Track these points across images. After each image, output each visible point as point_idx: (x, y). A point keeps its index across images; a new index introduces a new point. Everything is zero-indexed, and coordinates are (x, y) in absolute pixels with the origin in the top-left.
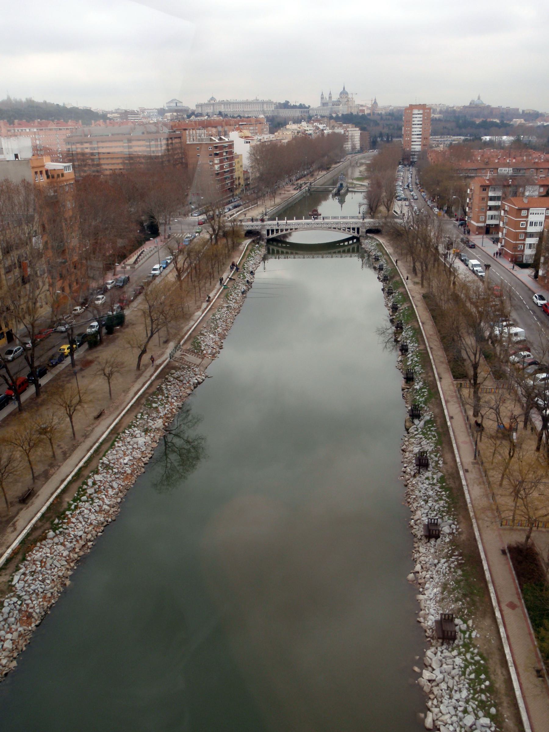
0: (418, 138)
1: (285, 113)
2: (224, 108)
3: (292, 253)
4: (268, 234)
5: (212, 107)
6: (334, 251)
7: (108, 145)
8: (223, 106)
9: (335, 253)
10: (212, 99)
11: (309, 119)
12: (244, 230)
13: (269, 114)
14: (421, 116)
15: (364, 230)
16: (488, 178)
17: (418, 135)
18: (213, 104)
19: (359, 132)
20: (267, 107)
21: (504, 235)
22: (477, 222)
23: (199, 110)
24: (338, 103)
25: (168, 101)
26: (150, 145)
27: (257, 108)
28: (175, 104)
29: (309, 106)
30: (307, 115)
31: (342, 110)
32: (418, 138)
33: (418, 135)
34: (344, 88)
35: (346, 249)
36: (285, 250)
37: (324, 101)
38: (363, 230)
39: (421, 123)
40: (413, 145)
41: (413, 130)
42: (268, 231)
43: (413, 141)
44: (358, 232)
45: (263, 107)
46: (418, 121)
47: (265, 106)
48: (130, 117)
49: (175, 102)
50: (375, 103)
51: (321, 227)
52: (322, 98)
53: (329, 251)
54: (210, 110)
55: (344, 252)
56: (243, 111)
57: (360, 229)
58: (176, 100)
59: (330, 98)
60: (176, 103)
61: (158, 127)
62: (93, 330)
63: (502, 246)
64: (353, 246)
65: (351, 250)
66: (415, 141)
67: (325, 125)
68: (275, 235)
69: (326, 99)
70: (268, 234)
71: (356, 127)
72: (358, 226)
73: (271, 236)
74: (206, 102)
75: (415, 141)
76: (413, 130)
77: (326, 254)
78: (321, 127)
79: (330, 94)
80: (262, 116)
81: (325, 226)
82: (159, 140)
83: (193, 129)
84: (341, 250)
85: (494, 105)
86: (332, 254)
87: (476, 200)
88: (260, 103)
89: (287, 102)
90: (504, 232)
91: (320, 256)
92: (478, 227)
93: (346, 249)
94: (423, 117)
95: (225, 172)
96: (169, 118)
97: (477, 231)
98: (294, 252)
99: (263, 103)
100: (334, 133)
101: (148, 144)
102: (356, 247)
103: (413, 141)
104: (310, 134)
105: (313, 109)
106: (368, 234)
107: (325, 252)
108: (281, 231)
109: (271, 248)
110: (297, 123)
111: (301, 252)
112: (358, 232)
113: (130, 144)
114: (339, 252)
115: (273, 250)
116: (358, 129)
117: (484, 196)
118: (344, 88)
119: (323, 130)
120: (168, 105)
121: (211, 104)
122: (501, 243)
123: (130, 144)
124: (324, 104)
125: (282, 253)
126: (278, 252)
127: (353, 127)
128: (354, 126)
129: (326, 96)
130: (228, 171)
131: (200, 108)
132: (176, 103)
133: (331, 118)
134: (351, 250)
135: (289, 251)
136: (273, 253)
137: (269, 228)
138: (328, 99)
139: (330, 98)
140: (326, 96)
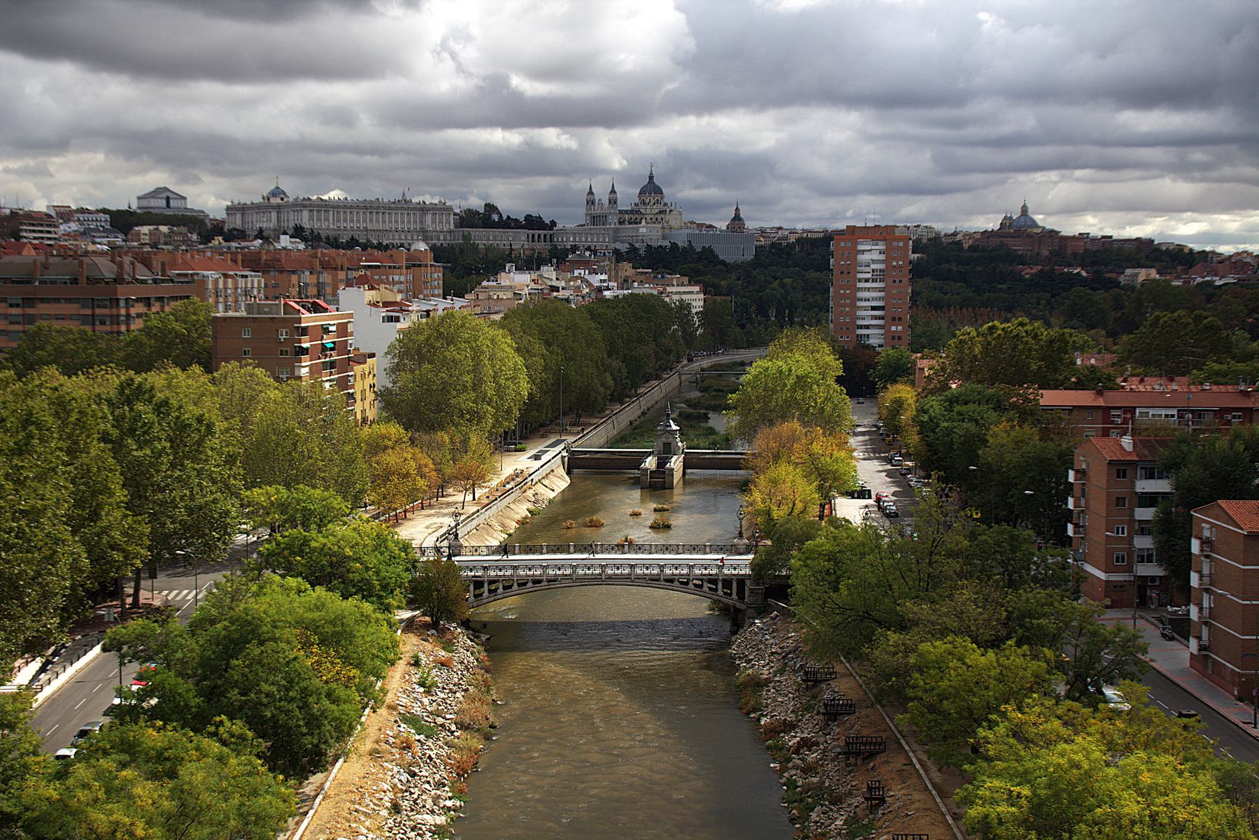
0: (876, 318)
1: (483, 238)
2: (311, 218)
5: (274, 215)
8: (305, 214)
10: (277, 192)
11: (560, 257)
13: (441, 241)
16: (306, 362)
17: (874, 308)
18: (278, 208)
19: (702, 296)
20: (434, 222)
21: (1206, 612)
23: (237, 222)
24: (634, 216)
25: (140, 194)
26: (93, 316)
27: (404, 222)
28: (164, 202)
29: (553, 223)
30: (548, 246)
31: (647, 233)
32: (876, 318)
33: (874, 308)
37: (597, 210)
41: (860, 295)
45: (421, 222)
47: (429, 218)
48: (28, 235)
49: (164, 195)
51: (628, 577)
52: (591, 203)
54: (268, 222)
56: (366, 229)
57: (748, 582)
58: (166, 189)
59: (613, 202)
60: (168, 199)
61: (121, 266)
63: (1201, 648)
67: (604, 277)
74: (258, 200)
76: (860, 295)
78: (596, 280)
79: (613, 191)
80: (422, 246)
82: (122, 303)
87: (1099, 505)
88: (414, 209)
89: (491, 208)
90: (1206, 604)
96: (146, 240)
99: (423, 209)
101: (89, 312)
104: (568, 300)
105: (563, 231)
110: (530, 269)
113: (29, 311)
116: (697, 289)
117: (1121, 491)
119: (600, 290)
120: (145, 203)
121: (273, 207)
122: (1199, 638)
123: (29, 311)
124: (596, 219)
127: (683, 285)
131: (239, 217)
132: (168, 199)
133: (619, 256)
139: (613, 202)
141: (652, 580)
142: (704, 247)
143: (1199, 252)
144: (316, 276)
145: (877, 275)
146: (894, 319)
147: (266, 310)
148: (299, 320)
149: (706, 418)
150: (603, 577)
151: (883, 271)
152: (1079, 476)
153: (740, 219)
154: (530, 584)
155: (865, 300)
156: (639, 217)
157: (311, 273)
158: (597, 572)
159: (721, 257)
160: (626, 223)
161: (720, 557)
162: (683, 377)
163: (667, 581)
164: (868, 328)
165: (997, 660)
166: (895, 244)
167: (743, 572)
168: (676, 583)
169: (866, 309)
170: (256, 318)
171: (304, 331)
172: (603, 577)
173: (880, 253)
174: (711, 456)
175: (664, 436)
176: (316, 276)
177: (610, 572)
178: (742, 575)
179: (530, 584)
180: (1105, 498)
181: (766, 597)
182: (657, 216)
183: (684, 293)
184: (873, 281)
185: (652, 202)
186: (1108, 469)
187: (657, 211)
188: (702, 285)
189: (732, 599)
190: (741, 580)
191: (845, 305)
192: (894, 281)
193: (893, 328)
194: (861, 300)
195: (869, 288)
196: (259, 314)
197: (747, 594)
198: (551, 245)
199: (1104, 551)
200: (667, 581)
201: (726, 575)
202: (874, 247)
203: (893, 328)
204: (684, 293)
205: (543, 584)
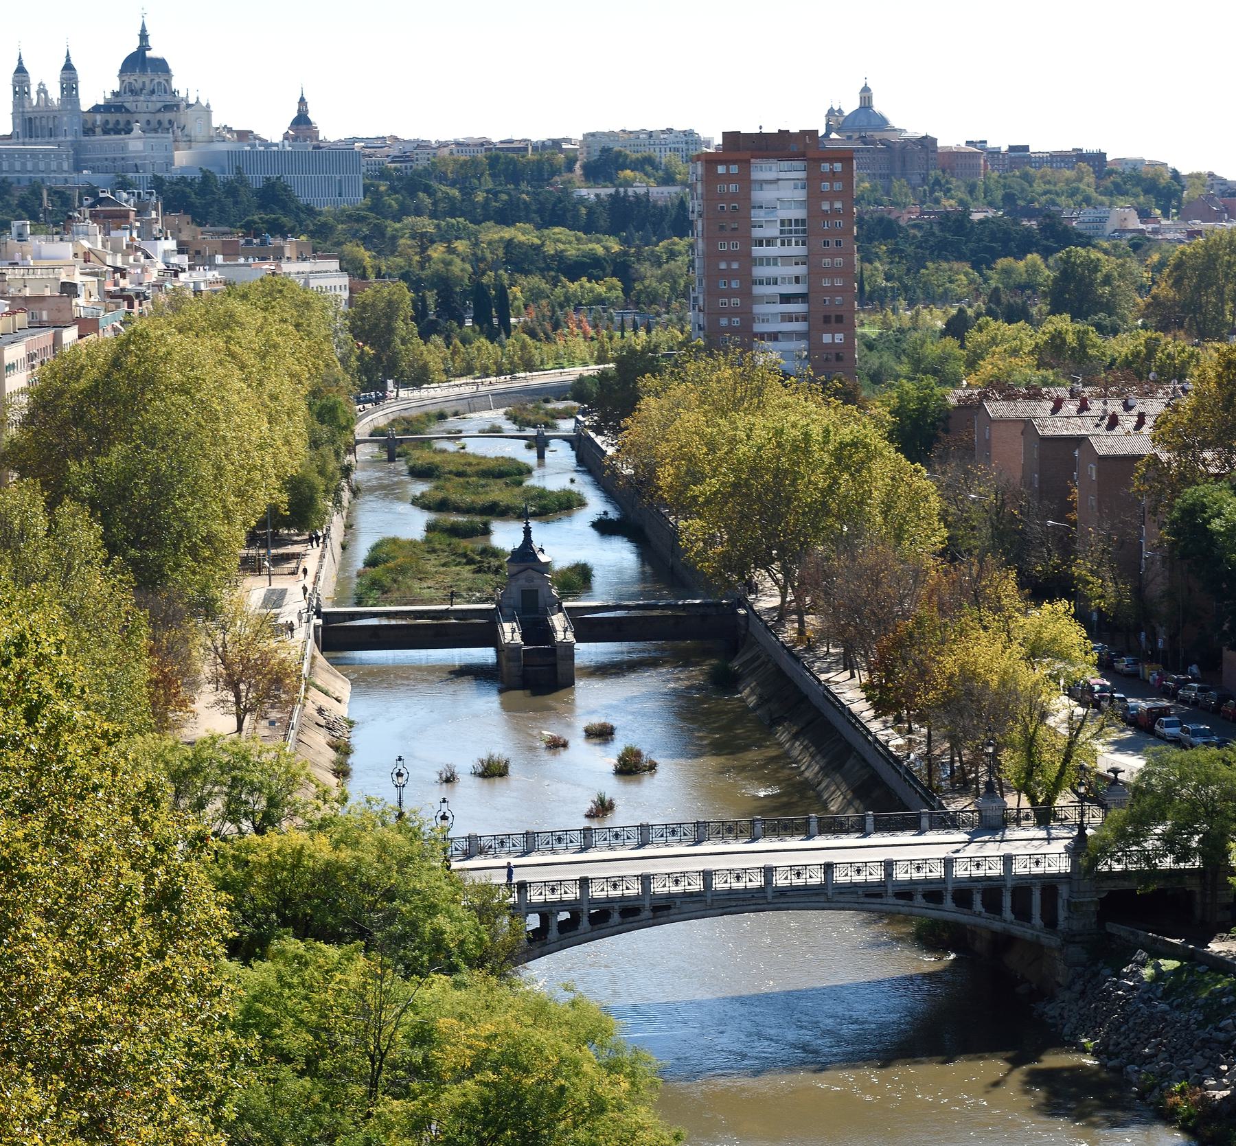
0: (788, 318)
17: (786, 299)
32: (788, 318)
33: (786, 299)
34: (144, 36)
41: (760, 272)
50: (302, 121)
57: (1064, 890)
69: (42, 90)
76: (760, 272)
85: (950, 138)
116: (334, 265)
118: (144, 36)
129: (45, 76)
138: (55, 93)
140: (45, 76)
141: (867, 896)
142: (268, 179)
143: (1190, 176)
145: (790, 232)
146: (827, 320)
149: (486, 532)
151: (803, 221)
153: (308, 122)
155: (768, 283)
156: (122, 118)
159: (303, 200)
160: (98, 130)
161: (503, 862)
163: (594, 919)
166: (826, 167)
167: (1054, 870)
172: (770, 894)
173: (796, 187)
174: (385, 622)
175: (524, 575)
178: (1053, 876)
179: (616, 918)
182: (159, 116)
184: (783, 244)
185: (149, 87)
187: (159, 105)
189: (1033, 927)
190: (1049, 883)
191: (730, 294)
192: (826, 244)
193: (827, 338)
194: (761, 283)
195: (775, 259)
197: (1062, 914)
201: (1021, 877)
202: (783, 175)
203: (827, 338)
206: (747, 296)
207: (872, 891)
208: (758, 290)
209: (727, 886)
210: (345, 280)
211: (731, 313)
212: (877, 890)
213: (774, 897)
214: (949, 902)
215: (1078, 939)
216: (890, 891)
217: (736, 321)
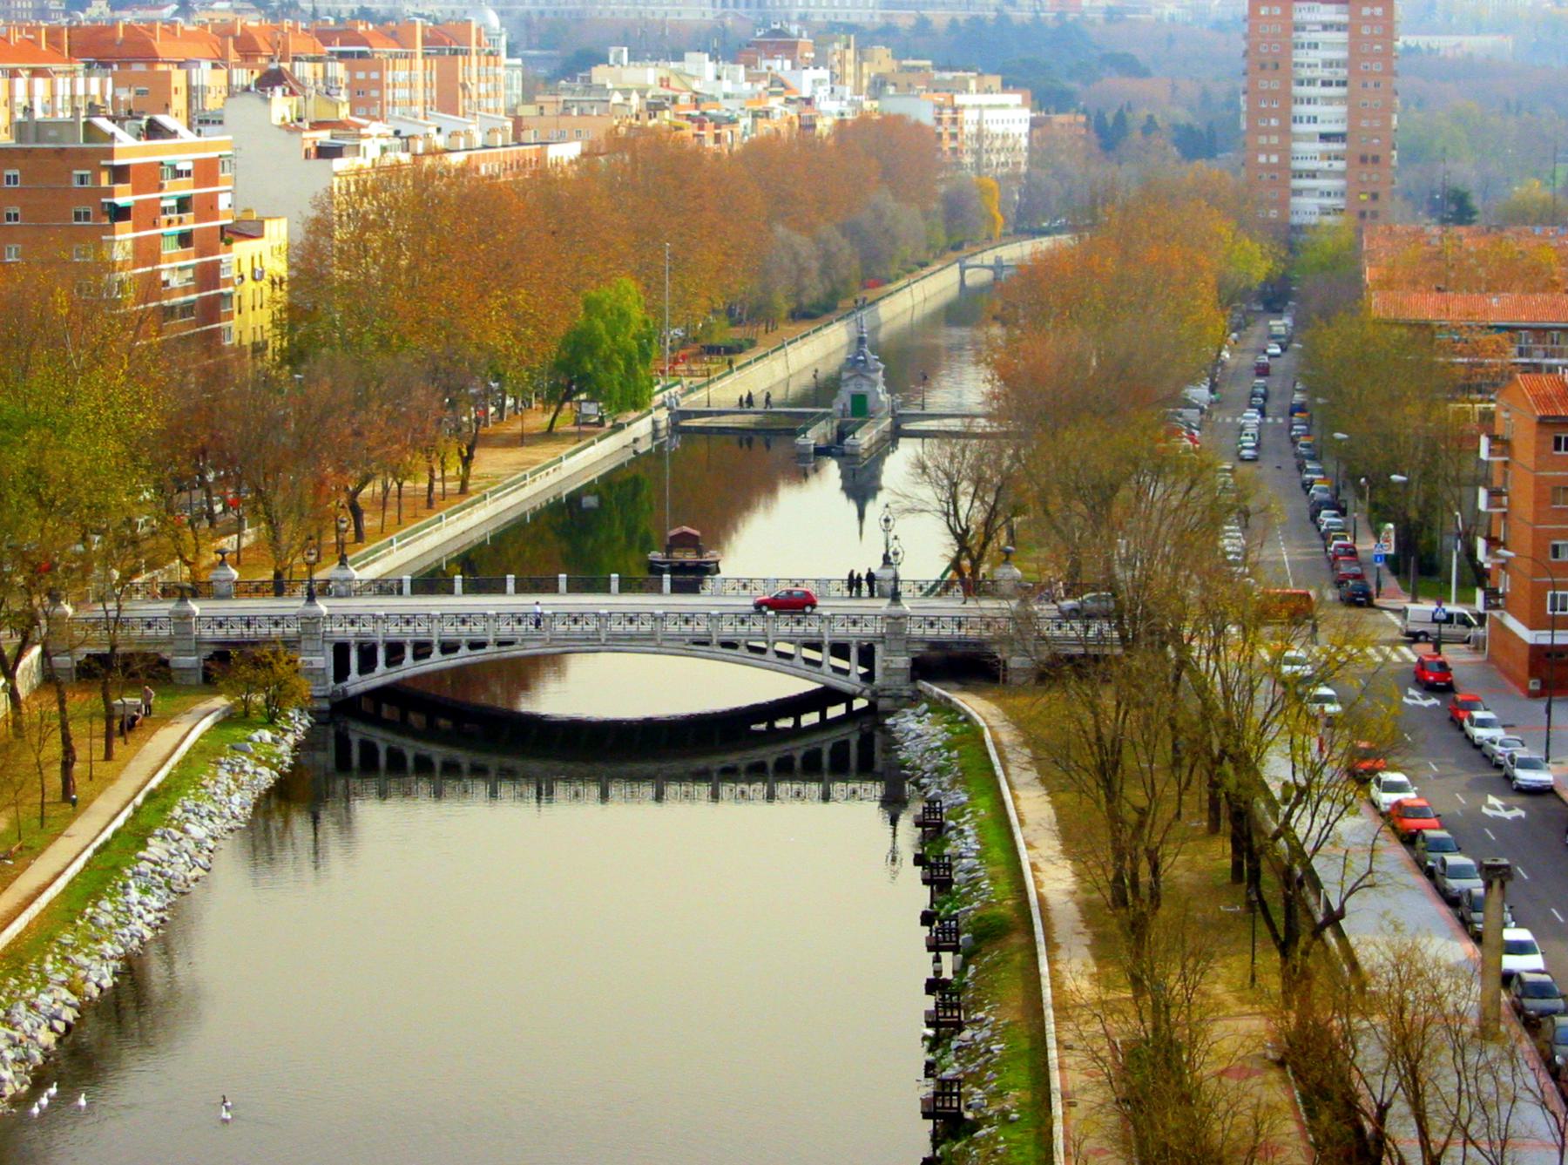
3: (479, 772)
4: (341, 672)
6: (732, 759)
7: (994, 103)
9: (730, 774)
12: (200, 642)
14: (1342, 37)
15: (902, 662)
17: (1325, 137)
22: (1532, 627)
34: (861, 516)
35: (825, 743)
36: (438, 753)
38: (893, 662)
39: (1343, 73)
40: (1298, 192)
42: (341, 650)
43: (1299, 175)
44: (343, 745)
46: (1328, 64)
51: (650, 637)
53: (701, 763)
55: (785, 769)
57: (879, 649)
62: (988, 605)
64: (837, 735)
65: (381, 655)
66: (1312, 175)
68: (382, 675)
70: (341, 672)
71: (1005, 86)
72: (871, 630)
73: (357, 683)
75: (1312, 175)
77: (680, 779)
81: (672, 629)
83: (35, 73)
84: (769, 755)
86: (718, 777)
91: (648, 790)
92: (1536, 649)
93: (798, 749)
94: (1353, 46)
95: (169, 312)
97: (1534, 671)
98: (493, 762)
100: (892, 123)
102: (854, 740)
103: (1299, 175)
106: (924, 685)
107: (678, 766)
108: (417, 657)
109: (355, 739)
111: (535, 765)
112: (343, 745)
114: (756, 772)
115: (369, 750)
116: (1015, 98)
118: (861, 516)
125: (424, 767)
126: (397, 764)
127: (989, 91)
128: (995, 81)
130: (187, 309)
134: (381, 655)
135: (464, 757)
136: (369, 766)
137: (349, 633)
144: (224, 72)
147: (52, 133)
148: (110, 154)
150: (603, 637)
152: (1498, 447)
154: (464, 650)
157: (214, 66)
158: (591, 628)
162: (968, 272)
164: (1314, 176)
165: (286, 516)
167: (870, 630)
168: (742, 650)
169: (1308, 137)
170: (30, 150)
171: (120, 174)
172: (603, 637)
176: (224, 72)
177: (616, 628)
180: (1532, 489)
181: (913, 679)
183: (990, 106)
186: (1538, 433)
188: (1028, 92)
191: (1268, 132)
196: (37, 141)
198: (761, 14)
199: (1528, 586)
200: (726, 645)
204: (990, 106)
205: (488, 649)
206: (1285, 132)
207: (697, 638)
208: (1297, 128)
209: (920, 632)
210: (1026, 114)
211: (1269, 150)
212: (703, 639)
213: (607, 640)
214: (437, 762)
215: (887, 693)
216: (715, 641)
217: (1274, 159)
